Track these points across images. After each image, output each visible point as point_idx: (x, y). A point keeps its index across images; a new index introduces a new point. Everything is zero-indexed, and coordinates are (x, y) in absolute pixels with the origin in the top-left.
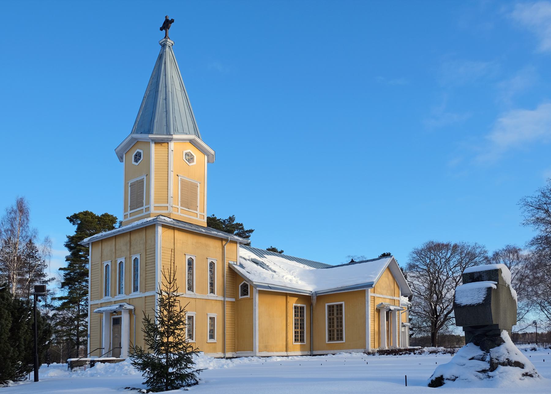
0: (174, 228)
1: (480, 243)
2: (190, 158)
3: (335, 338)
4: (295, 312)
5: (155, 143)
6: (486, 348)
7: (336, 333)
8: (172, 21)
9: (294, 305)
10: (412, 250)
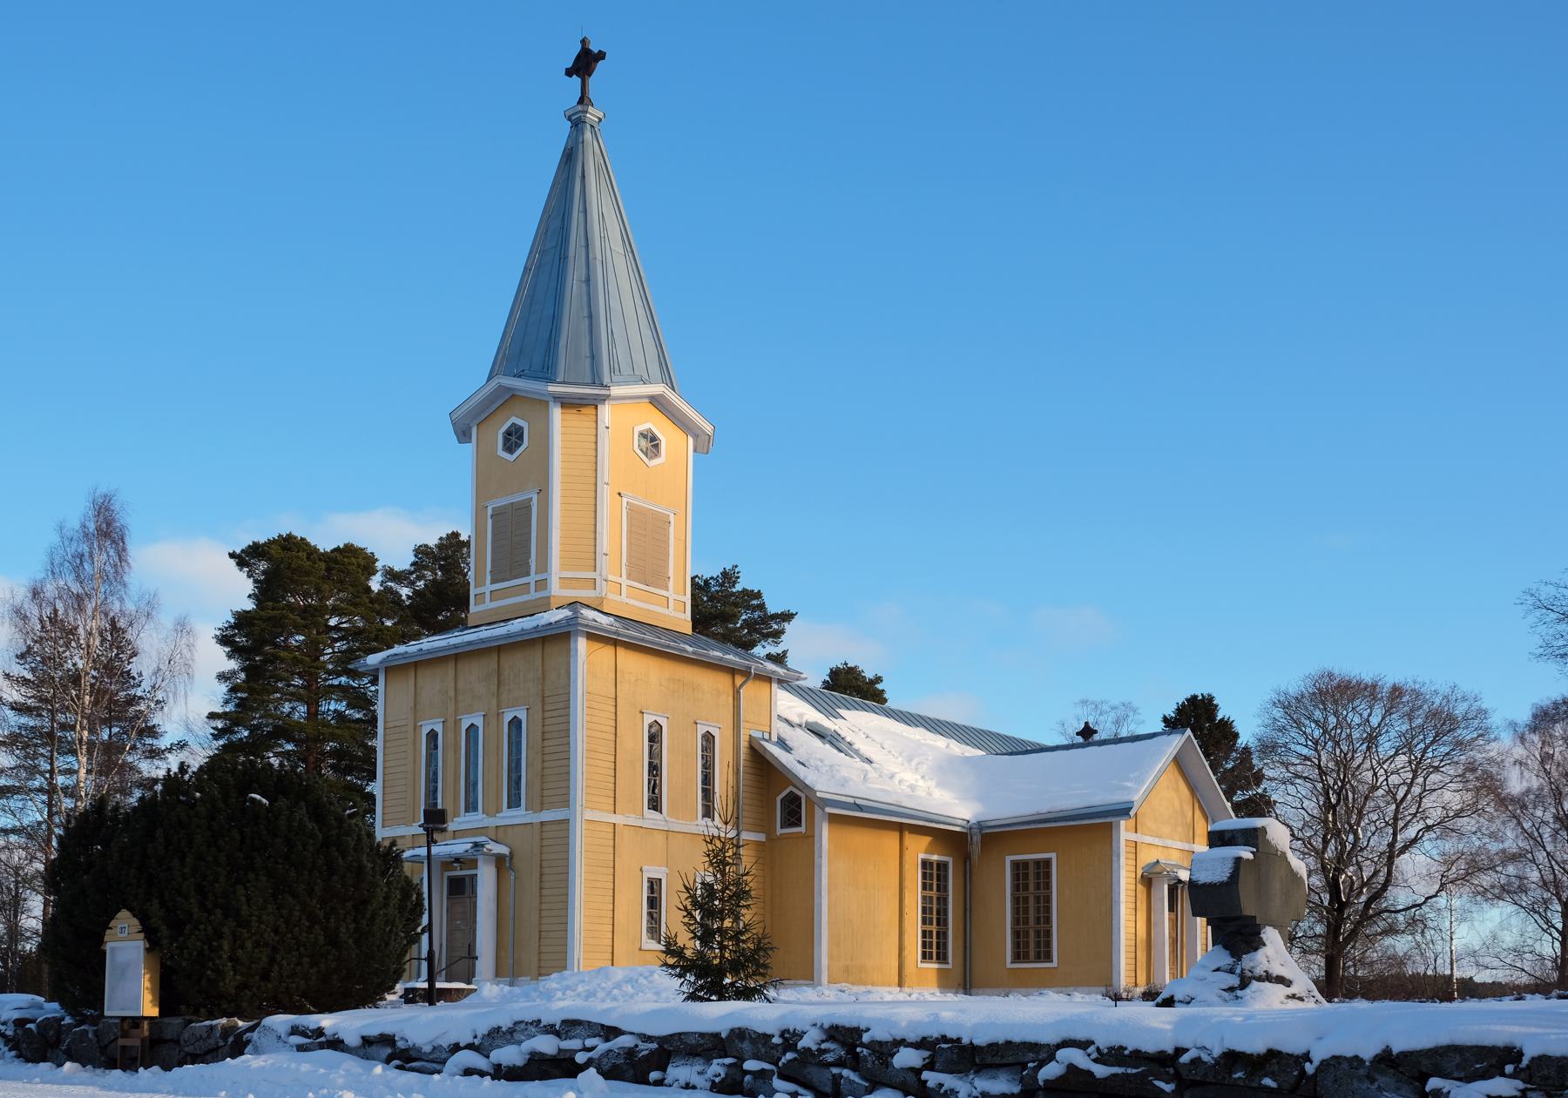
0: (615, 643)
1: (1466, 687)
2: (652, 443)
3: (1032, 954)
4: (924, 875)
5: (563, 406)
6: (1237, 954)
7: (1032, 941)
8: (601, 56)
9: (922, 856)
10: (1268, 695)
